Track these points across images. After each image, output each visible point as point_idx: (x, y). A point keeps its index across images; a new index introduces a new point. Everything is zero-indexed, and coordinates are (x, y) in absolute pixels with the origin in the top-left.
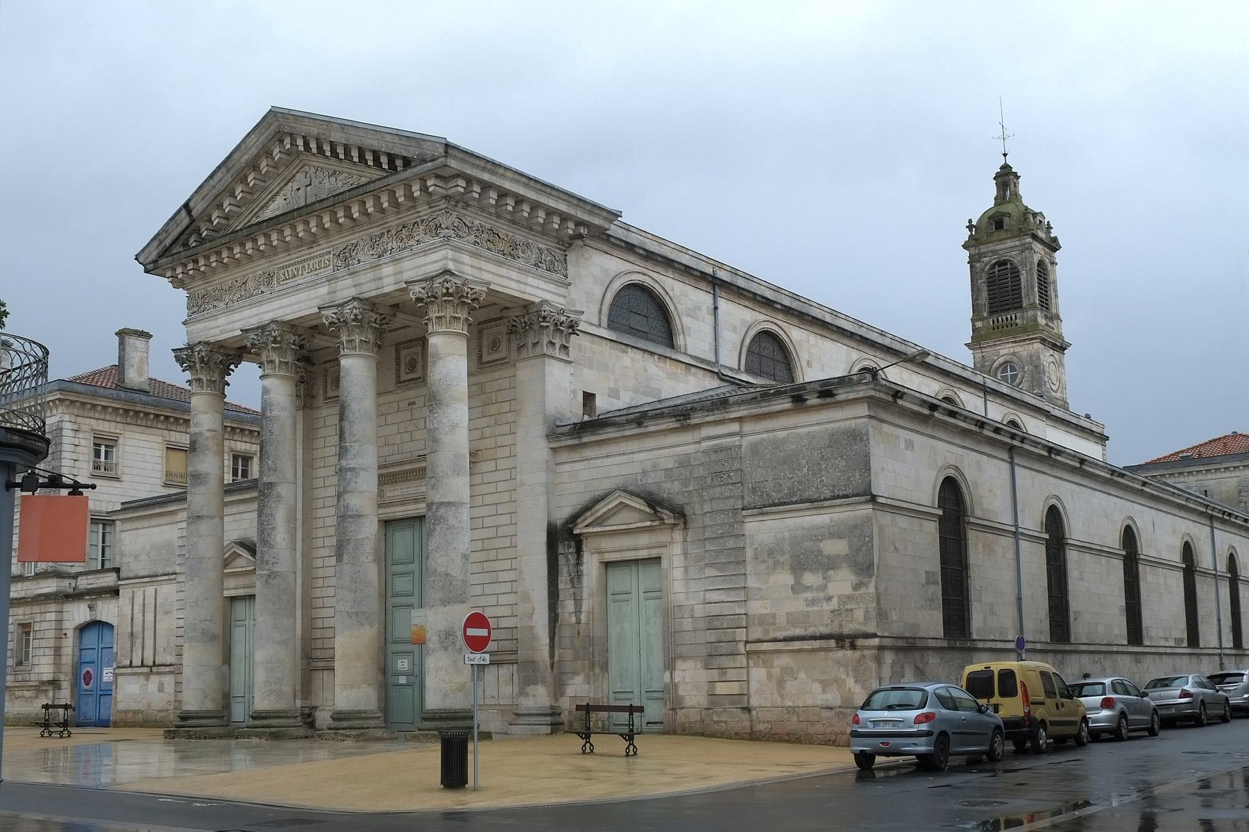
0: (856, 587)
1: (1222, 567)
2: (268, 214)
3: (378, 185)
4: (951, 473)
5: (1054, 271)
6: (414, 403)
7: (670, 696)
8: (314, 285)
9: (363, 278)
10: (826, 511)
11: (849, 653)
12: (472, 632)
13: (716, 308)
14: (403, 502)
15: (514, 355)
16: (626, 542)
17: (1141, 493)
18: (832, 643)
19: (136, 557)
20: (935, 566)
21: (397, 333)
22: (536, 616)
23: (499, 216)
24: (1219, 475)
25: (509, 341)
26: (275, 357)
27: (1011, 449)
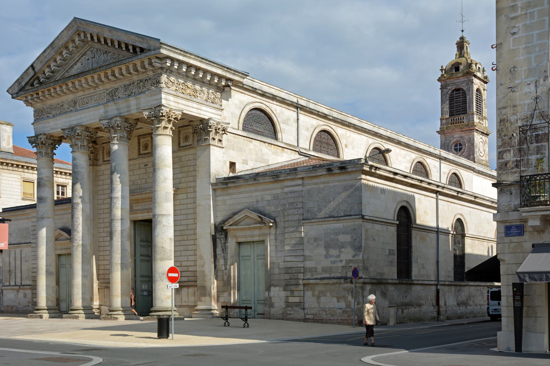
4: (404, 204)
6: (147, 165)
10: (341, 221)
12: (171, 275)
13: (298, 119)
15: (196, 144)
18: (342, 280)
20: (394, 246)
22: (206, 266)
25: (193, 136)
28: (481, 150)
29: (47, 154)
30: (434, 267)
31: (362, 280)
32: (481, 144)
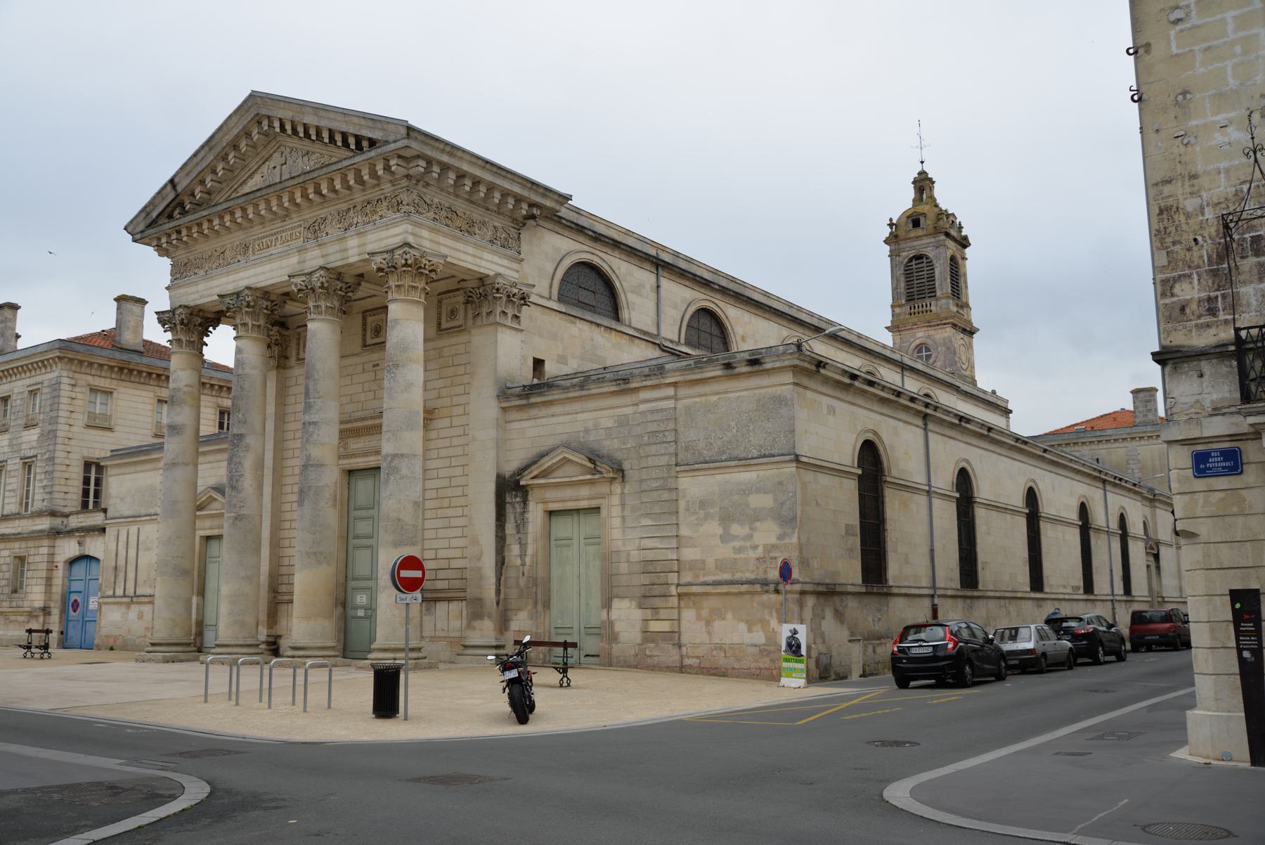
0: (781, 537)
1: (1114, 525)
2: (247, 189)
3: (345, 163)
4: (870, 436)
5: (965, 266)
7: (608, 632)
8: (284, 255)
9: (331, 249)
11: (774, 597)
14: (365, 454)
15: (470, 322)
16: (568, 493)
17: (1042, 458)
19: (122, 499)
20: (855, 520)
21: (357, 298)
23: (457, 196)
24: (1109, 445)
25: (466, 309)
26: (248, 320)
27: (925, 417)
28: (964, 358)
29: (190, 343)
30: (925, 561)
31: (797, 587)
32: (962, 348)
